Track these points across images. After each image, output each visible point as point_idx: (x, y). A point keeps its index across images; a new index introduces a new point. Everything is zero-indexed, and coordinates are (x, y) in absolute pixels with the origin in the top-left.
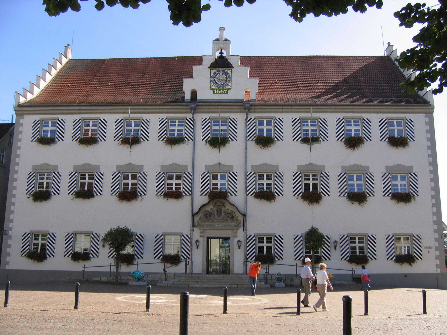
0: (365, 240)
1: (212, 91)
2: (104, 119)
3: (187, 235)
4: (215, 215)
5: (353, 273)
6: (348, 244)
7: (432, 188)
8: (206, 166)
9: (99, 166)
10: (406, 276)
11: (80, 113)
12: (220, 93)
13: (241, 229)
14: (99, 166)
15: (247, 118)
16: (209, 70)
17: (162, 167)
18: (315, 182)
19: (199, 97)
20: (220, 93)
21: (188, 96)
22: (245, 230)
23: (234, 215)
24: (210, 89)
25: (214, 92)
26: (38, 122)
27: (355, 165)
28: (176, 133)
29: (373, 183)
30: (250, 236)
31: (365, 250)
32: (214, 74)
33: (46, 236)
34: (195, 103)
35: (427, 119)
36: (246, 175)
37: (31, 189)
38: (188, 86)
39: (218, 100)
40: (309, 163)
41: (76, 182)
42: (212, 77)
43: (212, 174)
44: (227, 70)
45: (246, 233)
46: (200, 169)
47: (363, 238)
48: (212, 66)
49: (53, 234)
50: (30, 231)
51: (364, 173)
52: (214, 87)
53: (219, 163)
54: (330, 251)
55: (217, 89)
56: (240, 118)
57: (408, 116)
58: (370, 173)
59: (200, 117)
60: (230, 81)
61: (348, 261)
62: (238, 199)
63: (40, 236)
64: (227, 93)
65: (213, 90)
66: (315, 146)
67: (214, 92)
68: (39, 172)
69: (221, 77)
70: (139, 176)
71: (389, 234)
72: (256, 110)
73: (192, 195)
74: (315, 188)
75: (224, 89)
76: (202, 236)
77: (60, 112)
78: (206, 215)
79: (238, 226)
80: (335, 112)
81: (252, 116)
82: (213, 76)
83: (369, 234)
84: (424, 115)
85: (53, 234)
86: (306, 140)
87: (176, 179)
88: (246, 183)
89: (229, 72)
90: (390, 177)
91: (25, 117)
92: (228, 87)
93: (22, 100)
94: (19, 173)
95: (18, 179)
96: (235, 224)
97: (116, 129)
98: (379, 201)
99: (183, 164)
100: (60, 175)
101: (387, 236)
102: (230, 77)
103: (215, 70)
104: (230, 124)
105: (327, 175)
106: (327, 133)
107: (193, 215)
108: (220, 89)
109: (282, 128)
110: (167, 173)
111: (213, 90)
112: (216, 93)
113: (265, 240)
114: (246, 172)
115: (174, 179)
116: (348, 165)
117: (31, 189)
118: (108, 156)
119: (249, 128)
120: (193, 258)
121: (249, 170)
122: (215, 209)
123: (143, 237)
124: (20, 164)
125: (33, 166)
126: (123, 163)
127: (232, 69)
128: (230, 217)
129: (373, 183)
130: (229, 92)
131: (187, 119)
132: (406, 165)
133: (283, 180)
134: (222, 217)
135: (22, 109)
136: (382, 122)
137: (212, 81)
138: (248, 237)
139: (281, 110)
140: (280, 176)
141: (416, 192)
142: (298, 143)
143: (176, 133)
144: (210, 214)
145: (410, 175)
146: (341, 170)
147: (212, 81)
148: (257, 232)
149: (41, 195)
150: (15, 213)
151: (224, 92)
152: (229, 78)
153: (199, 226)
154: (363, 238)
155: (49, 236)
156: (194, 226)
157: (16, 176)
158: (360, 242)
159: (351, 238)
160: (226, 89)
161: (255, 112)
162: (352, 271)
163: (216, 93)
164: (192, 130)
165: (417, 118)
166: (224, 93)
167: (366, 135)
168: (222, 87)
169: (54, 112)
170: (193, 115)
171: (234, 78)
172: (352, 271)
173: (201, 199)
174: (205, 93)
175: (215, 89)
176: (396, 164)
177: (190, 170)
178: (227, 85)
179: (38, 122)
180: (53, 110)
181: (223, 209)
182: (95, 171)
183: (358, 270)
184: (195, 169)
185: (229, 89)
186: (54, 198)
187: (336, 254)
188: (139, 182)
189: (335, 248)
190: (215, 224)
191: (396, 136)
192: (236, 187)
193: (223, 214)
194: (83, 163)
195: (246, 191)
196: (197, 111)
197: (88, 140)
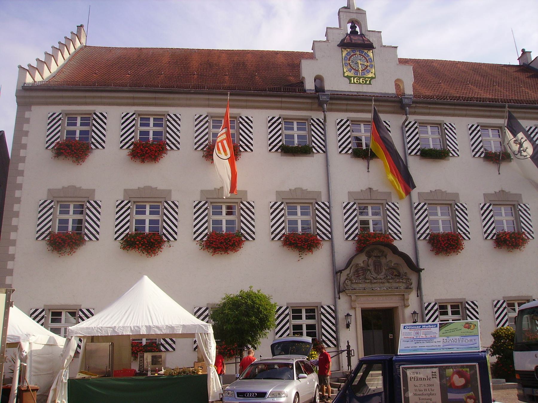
0: (316, 314)
1: (347, 80)
4: (372, 271)
6: (288, 321)
9: (170, 191)
11: (134, 105)
12: (360, 83)
14: (170, 191)
15: (406, 120)
16: (339, 49)
17: (278, 193)
20: (360, 83)
21: (310, 85)
22: (420, 295)
23: (401, 271)
24: (344, 76)
28: (151, 136)
29: (466, 220)
30: (429, 304)
31: (317, 331)
39: (357, 92)
44: (366, 51)
45: (421, 300)
46: (340, 199)
47: (457, 307)
50: (45, 306)
51: (157, 202)
52: (350, 74)
53: (370, 189)
58: (249, 203)
64: (370, 84)
66: (504, 166)
67: (350, 81)
68: (59, 200)
72: (417, 110)
73: (331, 239)
78: (357, 271)
79: (408, 288)
80: (465, 116)
81: (412, 118)
82: (345, 57)
83: (322, 304)
86: (288, 150)
89: (371, 54)
90: (426, 210)
91: (33, 108)
92: (370, 75)
93: (29, 80)
94: (22, 203)
95: (21, 214)
100: (100, 206)
103: (348, 50)
104: (168, 123)
105: (464, 207)
106: (179, 137)
107: (337, 273)
108: (360, 78)
109: (251, 132)
111: (349, 77)
112: (354, 83)
113: (304, 314)
119: (409, 136)
122: (371, 261)
124: (24, 186)
127: (374, 50)
128: (396, 273)
129: (466, 220)
131: (241, 117)
133: (253, 214)
134: (381, 276)
136: (126, 118)
139: (464, 112)
140: (464, 209)
141: (467, 233)
142: (348, 157)
143: (151, 136)
144: (365, 270)
145: (317, 206)
146: (347, 197)
147: (346, 64)
148: (49, 304)
149: (65, 241)
150: (15, 273)
151: (366, 81)
154: (457, 307)
155: (80, 313)
157: (16, 207)
158: (308, 318)
159: (294, 311)
160: (368, 78)
163: (354, 83)
164: (322, 136)
166: (366, 84)
167: (451, 148)
168: (362, 75)
171: (377, 62)
173: (344, 248)
174: (336, 83)
176: (66, 186)
177: (324, 199)
178: (369, 72)
180: (85, 97)
181: (383, 261)
184: (332, 198)
185: (372, 78)
186: (247, 248)
188: (87, 218)
189: (348, 326)
191: (77, 139)
192: (254, 226)
193: (384, 271)
194: (142, 186)
195: (414, 233)
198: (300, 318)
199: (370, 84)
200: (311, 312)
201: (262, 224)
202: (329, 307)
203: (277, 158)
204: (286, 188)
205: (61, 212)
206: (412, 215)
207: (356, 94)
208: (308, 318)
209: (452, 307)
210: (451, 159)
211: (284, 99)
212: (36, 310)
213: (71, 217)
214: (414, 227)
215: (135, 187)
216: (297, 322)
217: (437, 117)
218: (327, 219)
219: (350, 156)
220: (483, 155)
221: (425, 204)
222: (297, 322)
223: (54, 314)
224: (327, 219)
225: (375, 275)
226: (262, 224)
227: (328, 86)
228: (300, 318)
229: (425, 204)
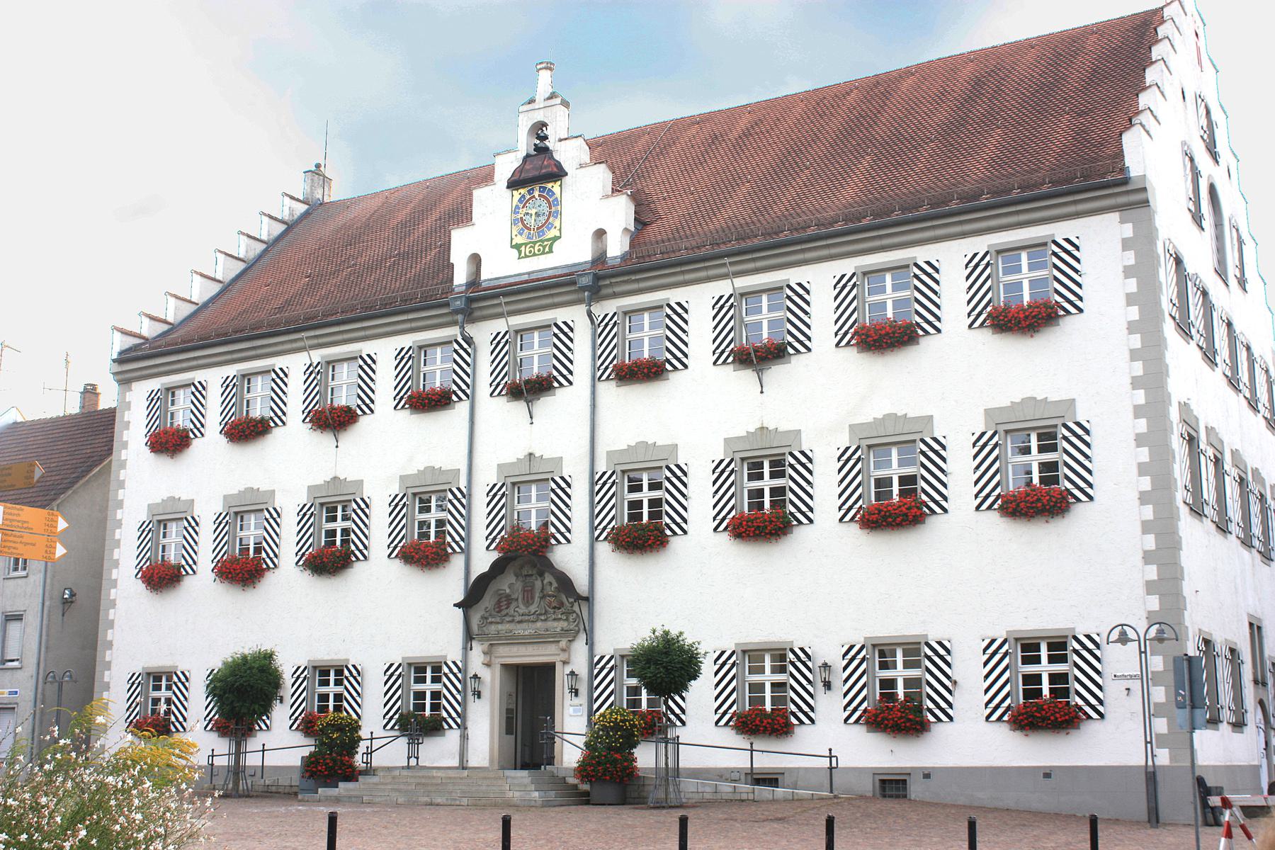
2: (1067, 240)
3: (454, 663)
5: (834, 765)
7: (1140, 465)
8: (727, 441)
9: (930, 418)
10: (1047, 774)
12: (535, 255)
13: (582, 637)
16: (509, 192)
17: (402, 478)
18: (756, 484)
19: (485, 275)
22: (590, 643)
25: (520, 253)
26: (849, 280)
27: (888, 417)
32: (520, 201)
33: (917, 652)
34: (482, 299)
35: (1128, 230)
36: (593, 483)
37: (856, 502)
38: (462, 244)
39: (529, 273)
40: (759, 425)
41: (733, 489)
42: (515, 211)
43: (515, 483)
46: (486, 476)
48: (513, 184)
49: (940, 643)
53: (531, 454)
54: (811, 695)
55: (526, 244)
56: (575, 315)
57: (1060, 231)
59: (484, 333)
60: (558, 214)
61: (734, 727)
62: (570, 558)
63: (332, 673)
64: (551, 251)
65: (517, 247)
66: (776, 373)
67: (520, 253)
69: (539, 205)
70: (1065, 438)
71: (992, 635)
72: (617, 289)
74: (778, 503)
75: (542, 241)
76: (488, 665)
77: (362, 334)
78: (499, 602)
80: (964, 235)
84: (1115, 216)
85: (940, 643)
87: (1040, 451)
88: (592, 507)
92: (553, 233)
96: (564, 624)
97: (970, 288)
98: (826, 534)
99: (449, 468)
101: (987, 642)
102: (558, 202)
103: (522, 191)
108: (535, 243)
110: (420, 495)
114: (592, 473)
115: (645, 487)
116: (870, 420)
117: (856, 502)
118: (293, 465)
120: (469, 724)
121: (601, 467)
122: (519, 586)
123: (359, 673)
125: (225, 497)
126: (319, 480)
130: (556, 245)
132: (1054, 397)
134: (533, 608)
135: (137, 359)
137: (514, 222)
138: (596, 659)
149: (162, 577)
151: (544, 247)
152: (554, 206)
153: (483, 637)
155: (791, 656)
156: (469, 636)
160: (548, 240)
161: (615, 295)
162: (831, 757)
165: (1099, 239)
166: (543, 253)
168: (537, 236)
169: (184, 365)
170: (462, 328)
172: (831, 757)
174: (502, 265)
175: (521, 245)
176: (1018, 400)
179: (849, 280)
182: (1059, 422)
183: (770, 756)
187: (830, 707)
190: (519, 626)
195: (593, 528)
196: (604, 292)
197: (759, 357)
198: (1037, 660)
199: (551, 251)
200: (1058, 648)
201: (701, 503)
202: (454, 663)
203: (986, 338)
204: (412, 470)
205: (751, 478)
206: (593, 494)
207: (526, 277)
208: (1052, 660)
209: (1051, 647)
210: (671, 375)
211: (411, 316)
212: (852, 647)
213: (1035, 459)
214: (593, 516)
215: (1006, 403)
216: (1031, 669)
217: (1027, 236)
218: (462, 515)
219: (855, 349)
220: (731, 359)
221: (995, 433)
222: (1031, 669)
223: (1025, 648)
224: (462, 515)
225: (522, 609)
226: (701, 503)
227: (488, 273)
228: (1037, 660)
229: (995, 433)
